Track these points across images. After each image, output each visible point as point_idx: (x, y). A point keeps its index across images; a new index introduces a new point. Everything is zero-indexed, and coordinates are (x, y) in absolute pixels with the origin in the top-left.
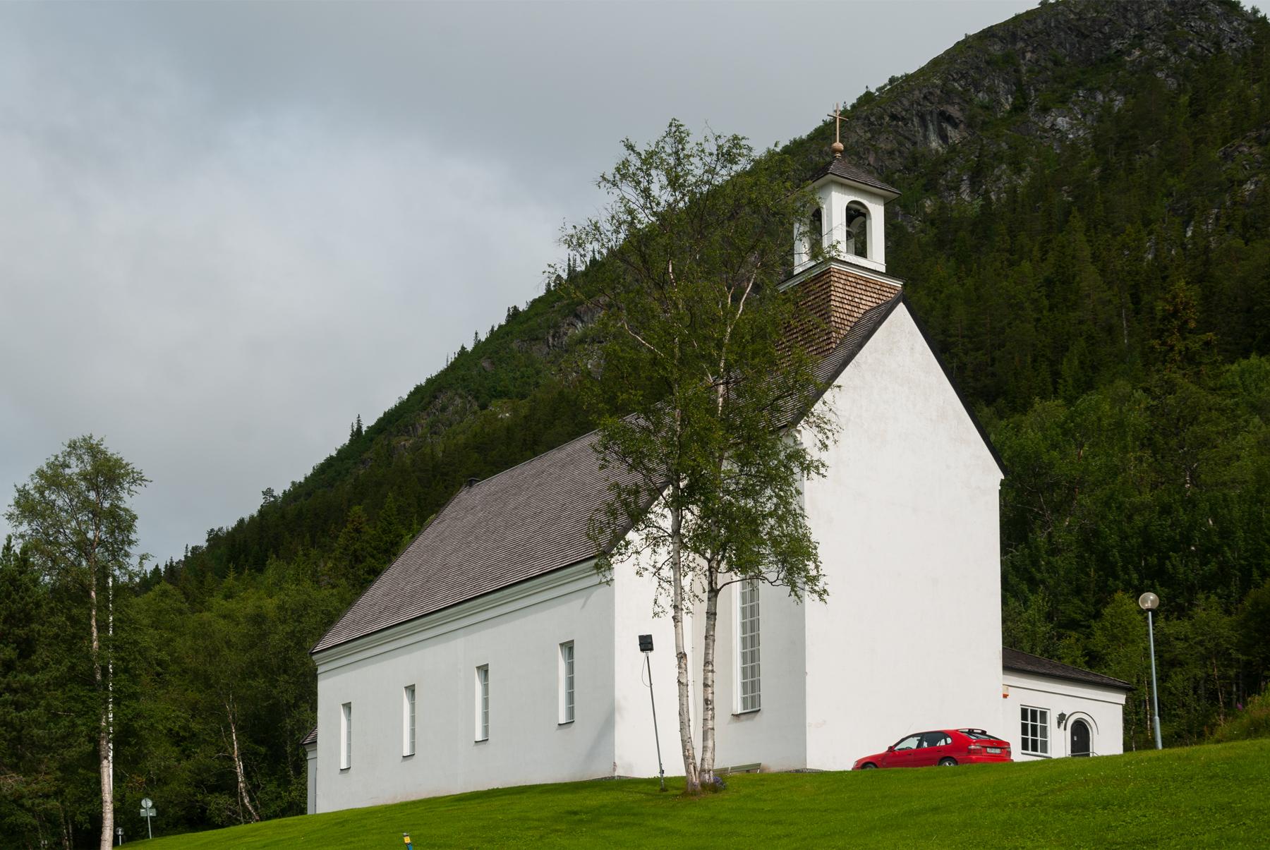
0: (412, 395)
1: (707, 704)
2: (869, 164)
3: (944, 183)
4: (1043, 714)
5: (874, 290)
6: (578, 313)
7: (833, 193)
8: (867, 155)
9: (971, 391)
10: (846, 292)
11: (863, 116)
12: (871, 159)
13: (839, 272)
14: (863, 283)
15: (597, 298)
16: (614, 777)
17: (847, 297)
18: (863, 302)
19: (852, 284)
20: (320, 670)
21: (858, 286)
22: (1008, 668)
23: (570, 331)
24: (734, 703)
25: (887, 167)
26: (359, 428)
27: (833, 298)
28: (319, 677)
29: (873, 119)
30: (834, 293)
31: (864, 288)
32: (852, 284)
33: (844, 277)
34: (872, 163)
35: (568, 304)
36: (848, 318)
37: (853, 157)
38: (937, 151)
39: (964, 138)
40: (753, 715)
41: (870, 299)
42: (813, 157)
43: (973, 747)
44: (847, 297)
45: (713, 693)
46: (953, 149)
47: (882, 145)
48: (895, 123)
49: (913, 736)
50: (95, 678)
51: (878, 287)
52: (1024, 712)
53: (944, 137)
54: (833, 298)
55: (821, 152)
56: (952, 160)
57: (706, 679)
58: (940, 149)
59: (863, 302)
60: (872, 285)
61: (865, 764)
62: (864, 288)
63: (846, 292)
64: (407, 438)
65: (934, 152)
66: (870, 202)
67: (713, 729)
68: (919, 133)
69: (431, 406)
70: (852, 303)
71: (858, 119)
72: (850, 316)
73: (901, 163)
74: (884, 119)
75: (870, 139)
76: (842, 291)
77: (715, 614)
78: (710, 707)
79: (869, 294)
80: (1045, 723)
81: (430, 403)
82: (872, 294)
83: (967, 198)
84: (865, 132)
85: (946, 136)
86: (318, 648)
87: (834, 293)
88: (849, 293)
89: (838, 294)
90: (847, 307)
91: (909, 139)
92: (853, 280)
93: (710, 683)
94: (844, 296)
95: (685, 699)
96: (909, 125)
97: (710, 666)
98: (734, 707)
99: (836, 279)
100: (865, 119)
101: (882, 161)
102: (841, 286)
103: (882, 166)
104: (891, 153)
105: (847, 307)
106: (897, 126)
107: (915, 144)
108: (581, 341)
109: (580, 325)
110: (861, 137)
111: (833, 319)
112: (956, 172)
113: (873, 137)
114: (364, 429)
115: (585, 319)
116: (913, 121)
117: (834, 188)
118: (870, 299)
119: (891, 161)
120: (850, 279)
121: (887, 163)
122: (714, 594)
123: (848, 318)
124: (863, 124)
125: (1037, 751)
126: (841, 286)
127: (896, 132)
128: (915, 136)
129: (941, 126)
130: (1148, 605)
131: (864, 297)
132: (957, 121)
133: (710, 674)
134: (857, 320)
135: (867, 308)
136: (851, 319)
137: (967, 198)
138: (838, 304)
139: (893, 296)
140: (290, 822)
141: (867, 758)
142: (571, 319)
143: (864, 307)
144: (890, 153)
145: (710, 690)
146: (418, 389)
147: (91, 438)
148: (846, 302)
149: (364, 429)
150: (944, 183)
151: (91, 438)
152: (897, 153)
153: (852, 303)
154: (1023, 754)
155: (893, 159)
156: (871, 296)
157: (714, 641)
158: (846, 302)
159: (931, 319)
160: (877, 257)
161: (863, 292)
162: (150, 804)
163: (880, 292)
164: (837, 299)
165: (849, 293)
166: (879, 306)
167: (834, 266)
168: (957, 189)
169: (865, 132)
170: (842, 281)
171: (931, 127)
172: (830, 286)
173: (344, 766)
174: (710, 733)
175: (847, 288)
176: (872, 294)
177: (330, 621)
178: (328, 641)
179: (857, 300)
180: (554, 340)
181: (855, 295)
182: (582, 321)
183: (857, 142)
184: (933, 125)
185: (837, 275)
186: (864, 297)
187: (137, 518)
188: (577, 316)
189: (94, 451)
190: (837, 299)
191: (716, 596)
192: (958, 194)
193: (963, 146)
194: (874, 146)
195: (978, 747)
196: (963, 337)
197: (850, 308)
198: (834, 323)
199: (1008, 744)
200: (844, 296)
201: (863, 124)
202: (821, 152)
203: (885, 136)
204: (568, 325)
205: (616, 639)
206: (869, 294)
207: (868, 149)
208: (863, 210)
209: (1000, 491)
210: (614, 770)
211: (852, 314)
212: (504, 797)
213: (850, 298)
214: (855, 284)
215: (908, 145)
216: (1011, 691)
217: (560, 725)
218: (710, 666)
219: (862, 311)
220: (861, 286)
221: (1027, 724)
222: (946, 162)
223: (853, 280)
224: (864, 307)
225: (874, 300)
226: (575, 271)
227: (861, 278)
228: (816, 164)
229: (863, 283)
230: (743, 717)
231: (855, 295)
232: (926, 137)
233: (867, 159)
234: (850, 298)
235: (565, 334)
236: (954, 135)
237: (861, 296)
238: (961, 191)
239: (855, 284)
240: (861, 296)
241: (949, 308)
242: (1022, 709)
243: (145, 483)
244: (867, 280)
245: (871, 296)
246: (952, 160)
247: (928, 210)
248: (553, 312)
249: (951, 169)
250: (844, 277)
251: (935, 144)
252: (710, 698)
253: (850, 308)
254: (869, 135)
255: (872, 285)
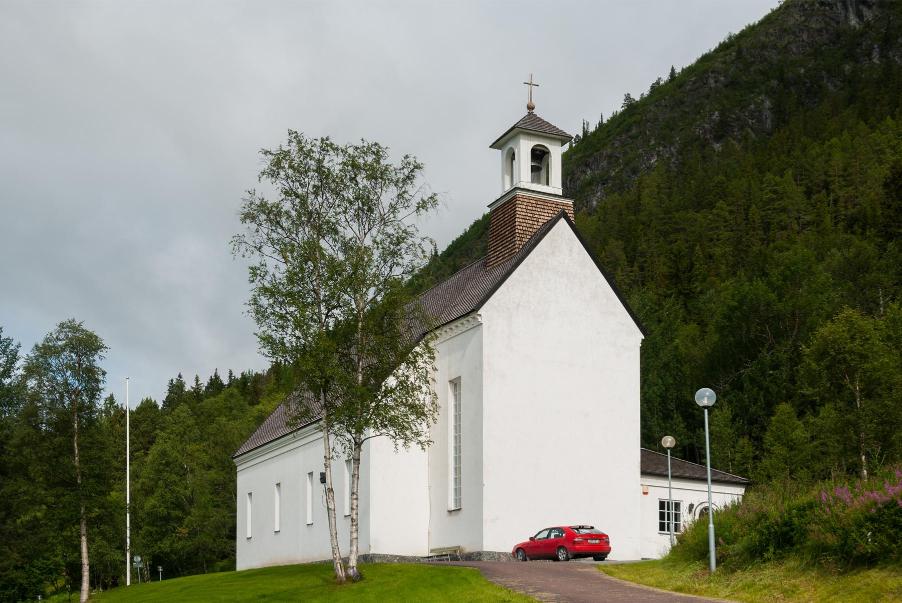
0: (472, 227)
1: (352, 522)
2: (803, 41)
3: (860, 51)
4: (677, 505)
5: (550, 208)
6: (588, 163)
7: (522, 141)
8: (801, 34)
9: (843, 217)
10: (528, 211)
11: (799, 5)
12: (805, 37)
13: (523, 197)
14: (541, 203)
15: (601, 151)
16: (369, 555)
17: (529, 215)
18: (542, 217)
19: (533, 205)
20: (239, 469)
21: (538, 206)
22: (644, 473)
23: (582, 177)
24: (449, 503)
25: (816, 42)
26: (436, 252)
27: (518, 216)
28: (238, 473)
29: (806, 6)
30: (519, 213)
31: (542, 207)
32: (533, 205)
33: (527, 200)
34: (805, 39)
35: (581, 157)
36: (529, 229)
37: (791, 36)
38: (855, 27)
39: (876, 16)
40: (458, 511)
41: (547, 215)
42: (761, 37)
43: (577, 540)
44: (529, 215)
45: (357, 514)
46: (868, 25)
47: (813, 26)
48: (823, 8)
49: (546, 529)
50: (77, 482)
51: (554, 206)
52: (662, 505)
53: (860, 16)
54: (518, 216)
55: (767, 33)
56: (866, 33)
57: (352, 504)
58: (857, 26)
59: (542, 217)
60: (549, 205)
61: (519, 549)
62: (542, 207)
63: (528, 211)
64: (468, 259)
65: (852, 28)
66: (551, 144)
67: (357, 538)
68: (841, 14)
69: (484, 236)
70: (532, 219)
71: (795, 7)
72: (530, 228)
73: (827, 38)
74: (814, 5)
75: (804, 22)
76: (525, 211)
77: (359, 460)
78: (355, 523)
79: (546, 211)
80: (660, 512)
81: (483, 233)
82: (549, 211)
83: (877, 62)
84: (801, 16)
85: (862, 15)
86: (237, 454)
87: (519, 213)
88: (531, 212)
89: (522, 213)
90: (529, 222)
91: (833, 19)
92: (534, 202)
93: (355, 507)
94: (526, 214)
95: (333, 519)
96: (834, 9)
97: (355, 495)
98: (449, 506)
99: (520, 203)
100: (801, 7)
101: (813, 38)
102: (524, 207)
103: (812, 41)
104: (820, 31)
105: (529, 222)
106: (825, 10)
107: (838, 23)
108: (590, 183)
109: (589, 172)
110: (797, 20)
111: (517, 231)
112: (869, 43)
113: (806, 20)
114: (439, 253)
115: (593, 167)
116: (837, 5)
117: (521, 136)
118: (547, 215)
119: (820, 37)
120: (531, 201)
121: (816, 39)
122: (357, 446)
123: (529, 229)
124: (799, 11)
125: (664, 530)
126: (524, 207)
127: (824, 15)
128: (838, 17)
129: (858, 8)
130: (668, 445)
131: (543, 214)
132: (870, 3)
133: (355, 501)
134: (536, 230)
135: (545, 221)
136: (531, 230)
137: (877, 62)
138: (521, 220)
139: (560, 210)
140: (186, 580)
141: (519, 545)
142: (582, 168)
143: (542, 221)
144: (818, 31)
145: (354, 512)
146: (477, 223)
147: (73, 320)
148: (528, 218)
149: (439, 253)
150: (860, 51)
151: (73, 320)
152: (825, 31)
153: (532, 219)
154: (659, 533)
155: (821, 35)
156: (548, 213)
157: (358, 478)
158: (528, 218)
159: (816, 164)
160: (556, 185)
161: (542, 210)
162: (139, 559)
163: (555, 209)
164: (521, 217)
165: (531, 212)
166: (545, 223)
167: (519, 193)
168: (869, 55)
169: (801, 16)
170: (525, 204)
171: (851, 9)
172: (516, 208)
173: (309, 522)
174: (355, 541)
175: (529, 208)
176: (549, 211)
177: (244, 438)
178: (244, 449)
179: (536, 216)
180: (570, 184)
181: (535, 213)
182: (591, 169)
183: (794, 24)
184: (852, 7)
185: (521, 199)
186: (543, 214)
187: (106, 373)
188: (587, 165)
189: (75, 328)
190: (521, 217)
191: (359, 447)
192: (870, 59)
193: (875, 22)
194: (807, 26)
195: (581, 540)
196: (839, 176)
197: (531, 222)
198: (517, 235)
199: (607, 536)
200: (526, 214)
201: (799, 11)
202: (767, 33)
203: (815, 18)
204: (581, 172)
205: (371, 459)
206: (546, 211)
207: (802, 29)
208: (546, 150)
209: (640, 347)
210: (370, 549)
211: (532, 226)
212: (260, 577)
213: (531, 215)
214: (535, 205)
215: (834, 24)
216: (650, 490)
217: (345, 516)
218: (355, 495)
219: (541, 224)
220: (540, 206)
221: (664, 512)
222: (862, 35)
223: (534, 202)
224: (542, 221)
225: (550, 215)
226: (587, 132)
227: (540, 200)
228: (763, 43)
229: (541, 203)
230: (453, 513)
231: (535, 213)
232: (847, 17)
233: (801, 37)
234: (531, 215)
235: (579, 179)
236: (868, 14)
237: (540, 213)
238: (872, 57)
239: (535, 205)
240: (540, 213)
241: (830, 154)
242: (660, 502)
243: (106, 350)
244: (545, 201)
245: (548, 213)
246: (866, 33)
247: (847, 73)
248: (571, 162)
249: (865, 40)
250: (527, 200)
251: (853, 21)
252: (354, 518)
253: (531, 222)
254: (803, 18)
255: (549, 205)
